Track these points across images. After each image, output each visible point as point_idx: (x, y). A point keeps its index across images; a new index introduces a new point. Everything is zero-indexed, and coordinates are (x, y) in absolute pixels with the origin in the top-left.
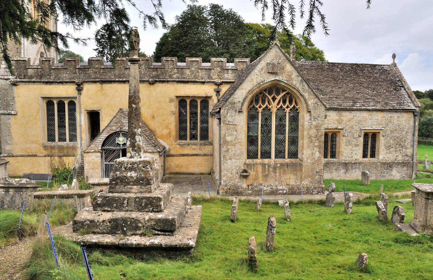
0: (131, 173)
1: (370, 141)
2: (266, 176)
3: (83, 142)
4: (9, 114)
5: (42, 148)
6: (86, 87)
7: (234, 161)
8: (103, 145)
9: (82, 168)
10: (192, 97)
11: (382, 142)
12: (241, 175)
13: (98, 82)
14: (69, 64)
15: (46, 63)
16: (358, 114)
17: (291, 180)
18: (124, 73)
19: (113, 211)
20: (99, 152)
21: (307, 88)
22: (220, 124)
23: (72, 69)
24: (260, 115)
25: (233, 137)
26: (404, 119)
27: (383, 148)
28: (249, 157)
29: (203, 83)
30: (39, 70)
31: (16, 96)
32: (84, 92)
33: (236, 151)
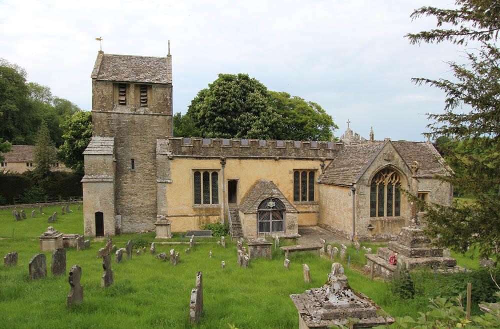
2: (383, 229)
5: (192, 209)
6: (228, 162)
7: (364, 219)
8: (258, 208)
13: (235, 158)
14: (215, 143)
18: (257, 152)
23: (217, 147)
24: (377, 187)
29: (312, 159)
30: (191, 148)
32: (226, 165)
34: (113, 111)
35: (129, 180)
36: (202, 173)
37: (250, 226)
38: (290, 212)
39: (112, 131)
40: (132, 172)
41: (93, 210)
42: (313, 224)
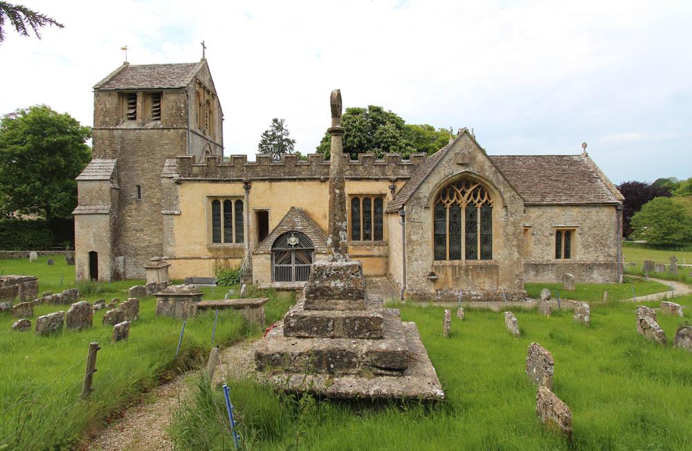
0: (336, 282)
1: (564, 238)
2: (457, 280)
3: (251, 243)
4: (172, 214)
5: (206, 250)
6: (254, 185)
7: (420, 262)
8: (274, 246)
9: (250, 271)
10: (366, 194)
11: (577, 241)
12: (428, 279)
13: (264, 180)
15: (212, 161)
16: (549, 210)
17: (486, 284)
18: (294, 171)
19: (312, 338)
20: (268, 254)
21: (503, 180)
22: (404, 221)
24: (448, 211)
25: (420, 236)
26: (605, 214)
27: (581, 247)
28: (436, 258)
29: (377, 180)
31: (179, 194)
32: (252, 190)
33: (422, 251)
34: (118, 127)
35: (134, 213)
36: (222, 202)
37: (261, 272)
38: (320, 253)
39: (115, 151)
40: (137, 201)
41: (86, 249)
42: (378, 274)
